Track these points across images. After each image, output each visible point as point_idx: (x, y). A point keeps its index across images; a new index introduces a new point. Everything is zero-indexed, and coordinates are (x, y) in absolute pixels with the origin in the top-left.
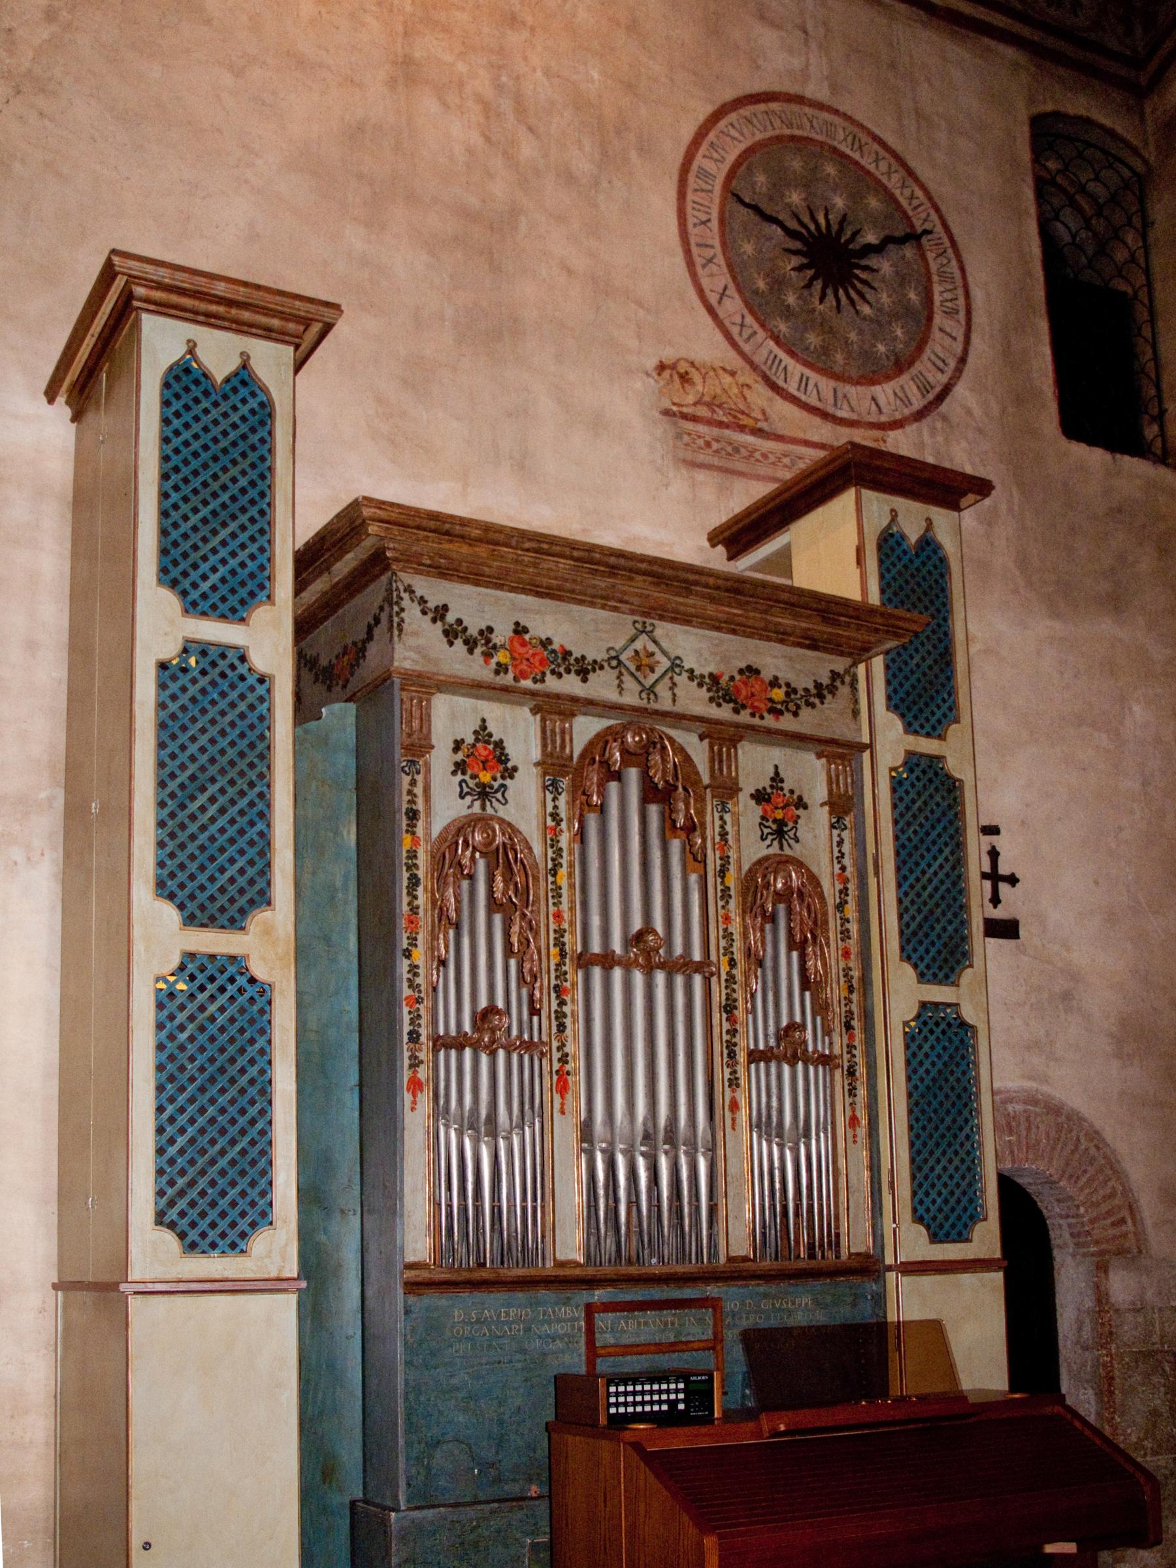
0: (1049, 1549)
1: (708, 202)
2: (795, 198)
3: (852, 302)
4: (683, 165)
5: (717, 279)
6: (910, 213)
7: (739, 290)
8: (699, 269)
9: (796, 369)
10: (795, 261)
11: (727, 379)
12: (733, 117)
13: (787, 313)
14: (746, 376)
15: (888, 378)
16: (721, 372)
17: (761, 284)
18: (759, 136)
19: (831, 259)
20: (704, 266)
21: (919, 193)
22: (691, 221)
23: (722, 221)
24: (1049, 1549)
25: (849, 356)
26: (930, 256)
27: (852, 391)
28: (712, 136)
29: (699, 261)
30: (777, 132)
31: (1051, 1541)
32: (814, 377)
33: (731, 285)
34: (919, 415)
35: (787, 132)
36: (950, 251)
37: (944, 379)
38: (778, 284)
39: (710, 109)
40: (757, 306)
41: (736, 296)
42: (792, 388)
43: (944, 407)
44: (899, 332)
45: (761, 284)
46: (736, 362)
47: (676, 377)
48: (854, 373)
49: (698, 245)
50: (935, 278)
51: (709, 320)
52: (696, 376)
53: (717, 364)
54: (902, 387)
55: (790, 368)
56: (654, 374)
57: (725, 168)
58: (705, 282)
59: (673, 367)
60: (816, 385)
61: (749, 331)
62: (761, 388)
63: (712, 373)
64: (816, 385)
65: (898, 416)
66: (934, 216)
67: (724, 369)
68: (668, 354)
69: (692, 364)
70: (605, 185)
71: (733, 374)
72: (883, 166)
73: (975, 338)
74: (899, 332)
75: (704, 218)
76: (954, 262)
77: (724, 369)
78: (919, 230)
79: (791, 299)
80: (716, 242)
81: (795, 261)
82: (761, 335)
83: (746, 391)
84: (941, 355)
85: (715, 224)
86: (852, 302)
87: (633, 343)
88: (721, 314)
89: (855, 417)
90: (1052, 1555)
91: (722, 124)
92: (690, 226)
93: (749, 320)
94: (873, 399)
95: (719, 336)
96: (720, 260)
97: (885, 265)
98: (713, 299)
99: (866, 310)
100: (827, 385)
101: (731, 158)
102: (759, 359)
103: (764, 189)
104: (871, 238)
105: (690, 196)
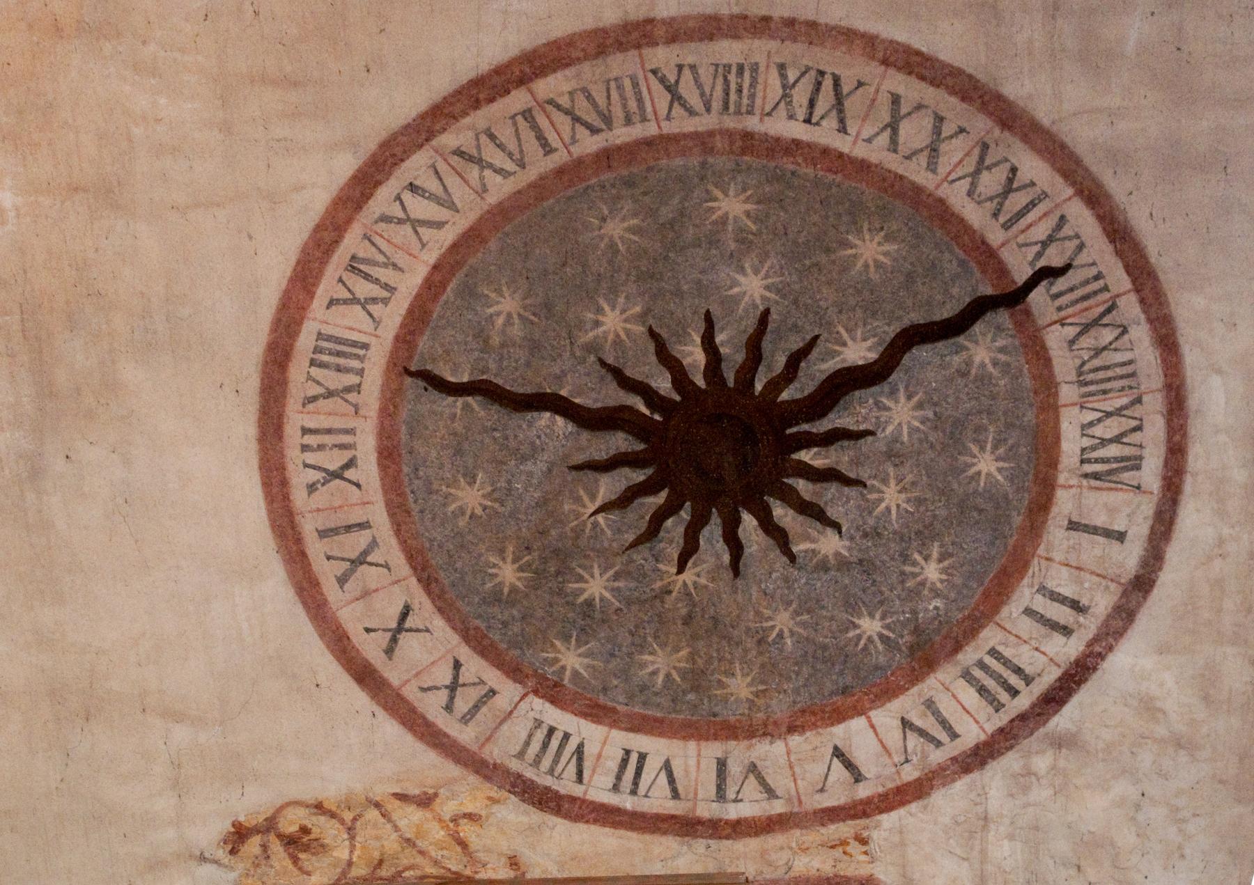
0: (789, 431)
1: (347, 418)
2: (615, 322)
3: (780, 537)
4: (272, 347)
5: (381, 594)
6: (995, 236)
7: (445, 608)
8: (331, 592)
9: (604, 743)
10: (609, 486)
11: (409, 817)
12: (417, 166)
13: (588, 620)
14: (467, 793)
15: (888, 693)
16: (393, 806)
17: (508, 574)
18: (500, 189)
19: (723, 446)
20: (342, 580)
21: (1033, 167)
22: (299, 478)
23: (388, 454)
24: (789, 431)
25: (769, 671)
26: (1055, 339)
27: (770, 752)
28: (352, 242)
29: (326, 572)
30: (560, 158)
31: (790, 426)
32: (656, 748)
33: (421, 600)
34: (979, 757)
35: (590, 144)
36: (1130, 307)
37: (1069, 649)
38: (554, 560)
39: (346, 165)
40: (503, 638)
41: (438, 623)
42: (599, 790)
43: (1064, 720)
44: (933, 572)
45: (508, 574)
46: (428, 766)
47: (277, 847)
48: (780, 707)
49: (323, 534)
50: (1068, 393)
51: (360, 698)
52: (327, 830)
53: (381, 791)
54: (930, 704)
55: (590, 750)
56: (221, 854)
57: (393, 316)
58: (351, 617)
59: (270, 825)
60: (667, 766)
61: (474, 694)
62: (513, 814)
63: (373, 814)
64: (667, 766)
65: (910, 774)
66: (1082, 219)
67: (402, 797)
68: (251, 803)
69: (319, 807)
70: (59, 465)
71: (425, 801)
72: (914, 132)
73: (1193, 518)
74: (933, 572)
75: (333, 461)
76: (1141, 334)
77: (402, 797)
78: (1021, 274)
79: (596, 587)
80: (379, 516)
81: (609, 486)
82: (508, 691)
83: (467, 830)
84: (1067, 591)
85: (368, 470)
86: (780, 537)
87: (164, 804)
88: (393, 674)
89: (778, 807)
90: (791, 435)
91: (382, 200)
92: (299, 497)
93: (475, 666)
94: (838, 753)
95: (390, 729)
96: (391, 550)
97: (896, 413)
98: (371, 649)
99: (830, 544)
100: (694, 760)
101: (410, 283)
102: (501, 751)
103: (517, 331)
104: (858, 352)
105: (295, 419)
